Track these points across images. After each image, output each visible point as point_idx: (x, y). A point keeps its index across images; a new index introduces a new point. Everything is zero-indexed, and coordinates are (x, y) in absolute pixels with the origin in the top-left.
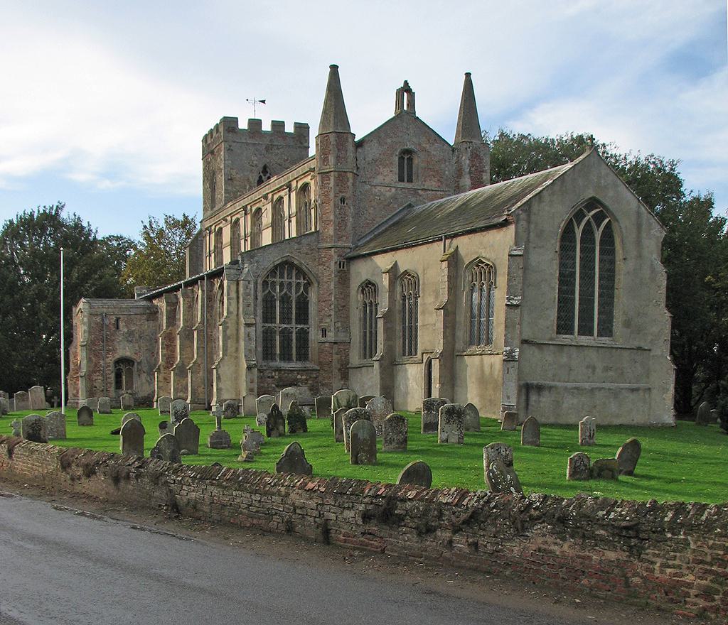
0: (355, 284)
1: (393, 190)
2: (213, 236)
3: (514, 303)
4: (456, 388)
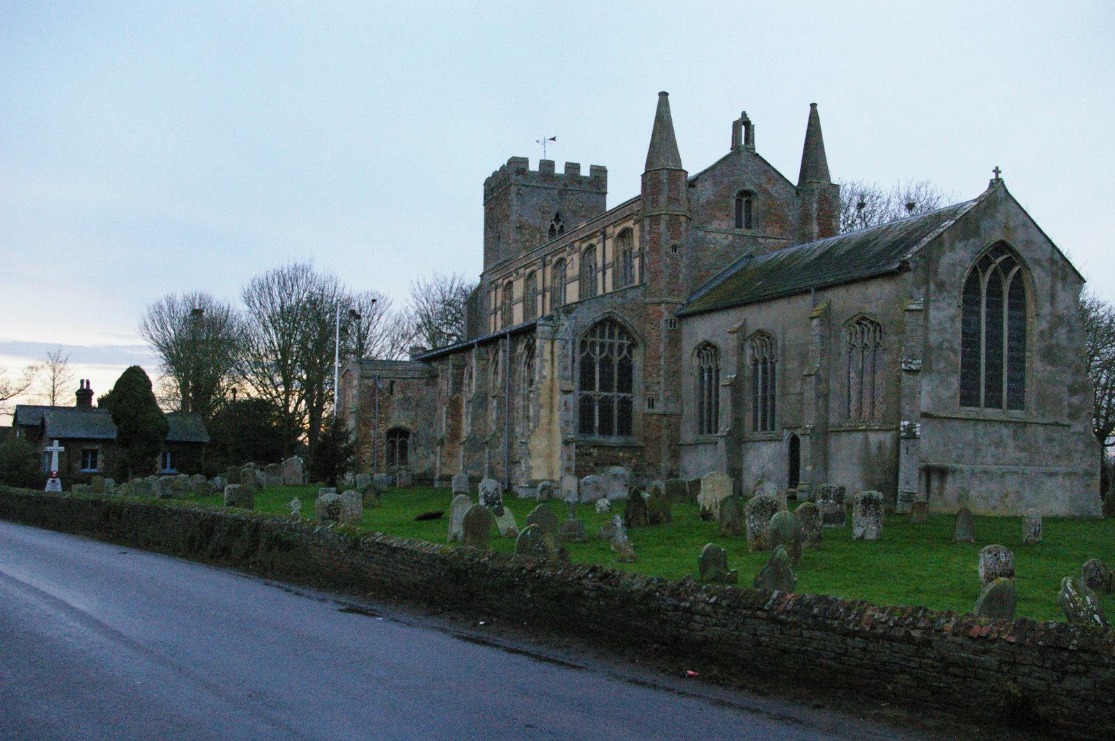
0: (688, 347)
1: (730, 237)
2: (500, 291)
3: (913, 367)
4: (830, 472)
